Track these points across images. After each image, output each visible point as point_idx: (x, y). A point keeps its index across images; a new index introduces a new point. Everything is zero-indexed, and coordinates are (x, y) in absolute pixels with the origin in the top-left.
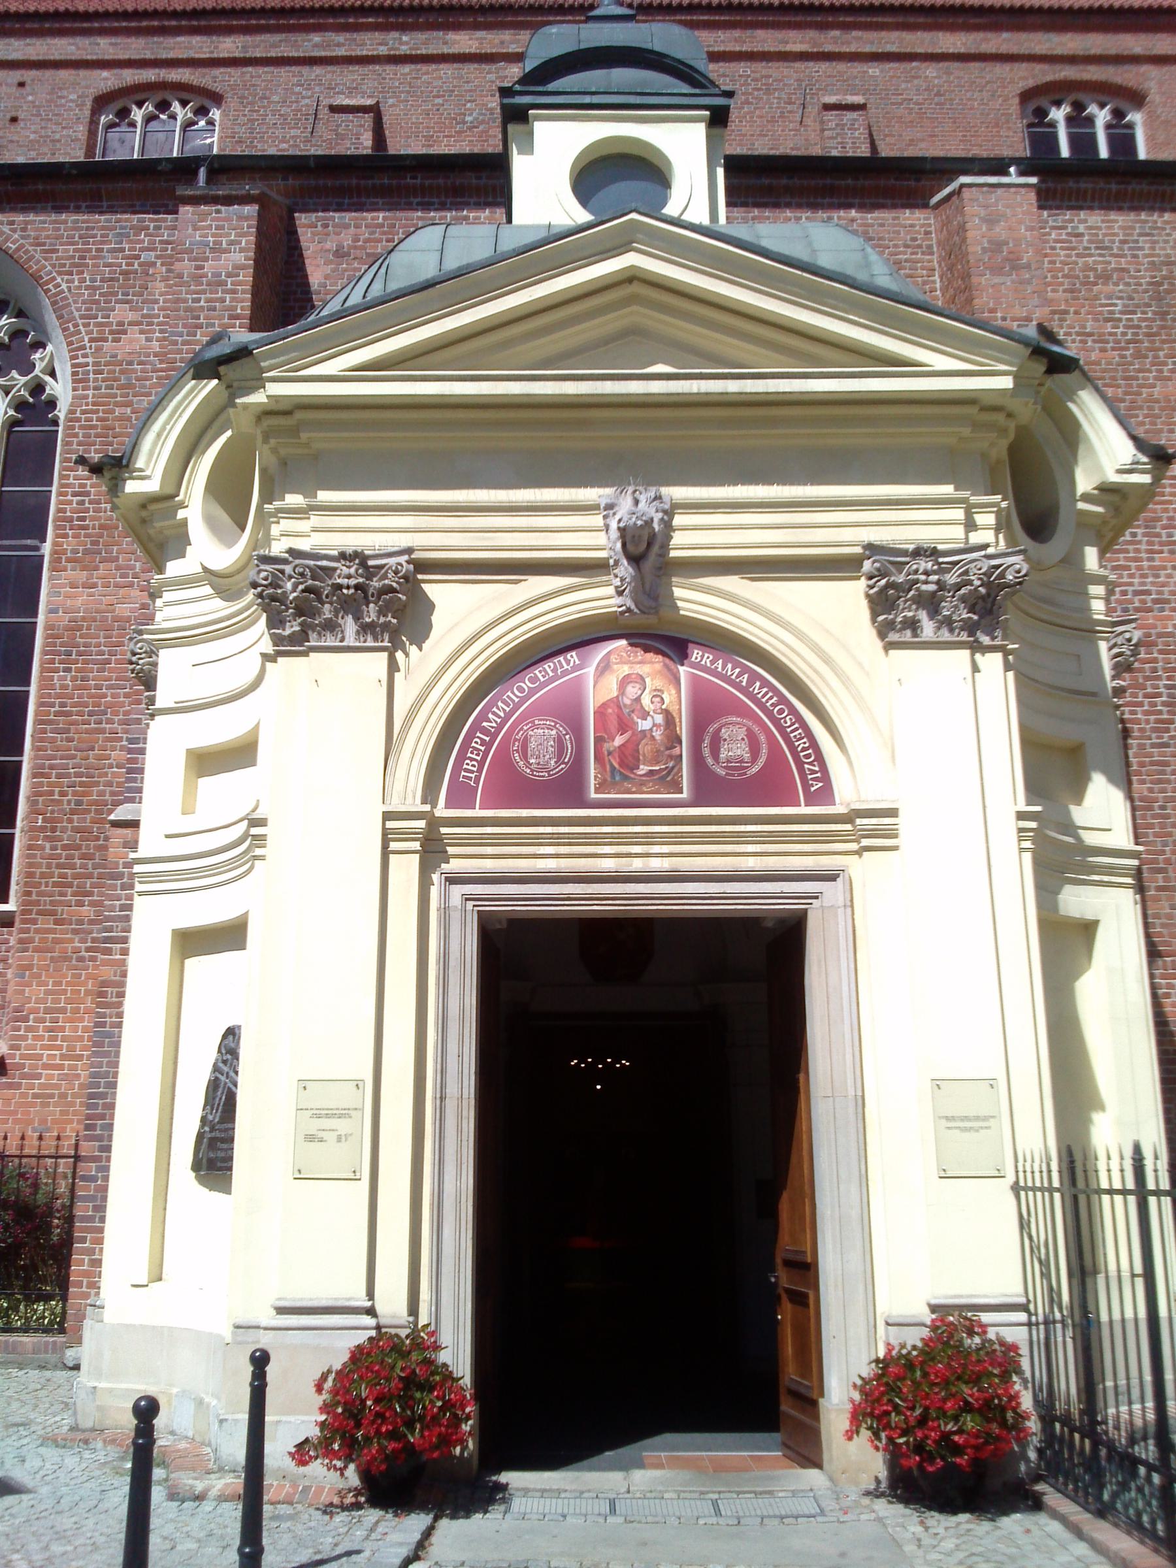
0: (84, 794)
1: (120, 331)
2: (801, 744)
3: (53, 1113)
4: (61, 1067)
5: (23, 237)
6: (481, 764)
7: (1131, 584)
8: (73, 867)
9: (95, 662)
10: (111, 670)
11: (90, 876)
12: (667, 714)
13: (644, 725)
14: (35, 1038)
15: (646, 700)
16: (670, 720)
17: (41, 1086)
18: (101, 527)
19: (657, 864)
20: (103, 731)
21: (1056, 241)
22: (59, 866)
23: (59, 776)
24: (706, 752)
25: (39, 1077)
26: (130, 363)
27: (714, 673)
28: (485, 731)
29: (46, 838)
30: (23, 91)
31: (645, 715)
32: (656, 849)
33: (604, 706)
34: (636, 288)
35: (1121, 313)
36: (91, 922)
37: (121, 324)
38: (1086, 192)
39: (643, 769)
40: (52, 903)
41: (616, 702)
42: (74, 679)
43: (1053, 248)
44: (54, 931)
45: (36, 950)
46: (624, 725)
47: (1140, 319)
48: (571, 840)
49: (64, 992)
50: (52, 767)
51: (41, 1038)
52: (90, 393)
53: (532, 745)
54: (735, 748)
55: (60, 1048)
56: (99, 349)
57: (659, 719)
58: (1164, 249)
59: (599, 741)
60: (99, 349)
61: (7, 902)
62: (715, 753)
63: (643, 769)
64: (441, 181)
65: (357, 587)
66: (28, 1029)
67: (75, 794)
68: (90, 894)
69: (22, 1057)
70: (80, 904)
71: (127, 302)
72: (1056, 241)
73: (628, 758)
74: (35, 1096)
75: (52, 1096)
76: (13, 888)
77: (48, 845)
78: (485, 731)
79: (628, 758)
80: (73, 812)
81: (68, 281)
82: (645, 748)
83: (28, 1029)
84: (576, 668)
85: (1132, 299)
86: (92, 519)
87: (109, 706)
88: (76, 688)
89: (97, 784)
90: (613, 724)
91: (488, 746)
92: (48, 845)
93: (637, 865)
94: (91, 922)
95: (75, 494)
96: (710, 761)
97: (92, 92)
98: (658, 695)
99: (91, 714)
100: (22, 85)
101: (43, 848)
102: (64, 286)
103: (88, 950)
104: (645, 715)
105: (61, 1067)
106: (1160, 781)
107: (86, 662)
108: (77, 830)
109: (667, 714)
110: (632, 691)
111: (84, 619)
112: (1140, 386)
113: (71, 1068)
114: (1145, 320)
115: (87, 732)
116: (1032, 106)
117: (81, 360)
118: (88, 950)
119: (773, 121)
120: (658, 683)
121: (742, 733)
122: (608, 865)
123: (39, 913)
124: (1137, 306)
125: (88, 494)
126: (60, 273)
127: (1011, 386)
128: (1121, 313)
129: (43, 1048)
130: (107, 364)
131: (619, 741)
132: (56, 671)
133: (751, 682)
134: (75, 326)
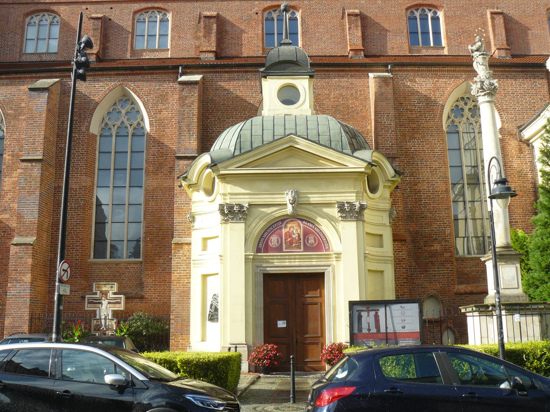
0: (158, 232)
1: (160, 112)
2: (324, 240)
3: (156, 309)
4: (158, 298)
5: (134, 85)
6: (263, 244)
7: (416, 176)
8: (157, 250)
9: (159, 199)
10: (163, 201)
11: (161, 252)
12: (298, 234)
13: (294, 236)
14: (151, 291)
15: (294, 231)
16: (299, 235)
17: (153, 303)
18: (159, 164)
19: (297, 264)
20: (162, 216)
21: (401, 84)
22: (154, 250)
23: (152, 228)
24: (306, 242)
25: (152, 300)
26: (164, 120)
27: (307, 225)
28: (264, 238)
29: (150, 243)
30: (112, 10)
31: (294, 234)
32: (296, 261)
33: (286, 233)
34: (292, 148)
35: (417, 104)
36: (163, 264)
37: (161, 109)
38: (409, 70)
39: (294, 245)
40: (153, 259)
41: (289, 232)
42: (154, 203)
43: (400, 86)
44: (153, 266)
45: (149, 270)
46: (290, 236)
47: (421, 105)
48: (280, 259)
49: (157, 281)
50: (150, 225)
51: (152, 291)
52: (154, 128)
53: (272, 240)
54: (311, 241)
55: (157, 294)
56: (156, 116)
57: (297, 235)
58: (429, 85)
59: (285, 239)
60: (156, 116)
61: (140, 258)
62: (308, 242)
63: (294, 245)
64: (242, 69)
65: (239, 211)
66: (149, 289)
67: (156, 232)
68: (162, 257)
69: (148, 296)
70: (159, 259)
71: (162, 103)
72: (401, 84)
73: (291, 243)
74: (152, 305)
75: (156, 305)
76: (141, 255)
77: (151, 245)
78: (264, 238)
79: (291, 243)
80: (156, 237)
81: (147, 98)
82: (294, 241)
83: (149, 289)
84: (281, 225)
85: (420, 99)
86: (157, 162)
87: (164, 210)
88: (155, 205)
89: (162, 229)
90: (288, 236)
91: (264, 241)
92: (151, 245)
93: (293, 264)
94: (163, 264)
95: (152, 155)
96: (307, 243)
97: (132, 10)
98: (297, 230)
99: (159, 212)
100: (111, 8)
101: (150, 246)
102: (146, 99)
103: (162, 270)
104: (294, 234)
105: (158, 298)
106: (421, 226)
107: (157, 199)
108: (157, 241)
109: (298, 234)
110: (292, 229)
111: (156, 188)
112: (421, 124)
113: (160, 298)
114: (423, 105)
115: (159, 216)
116: (409, 11)
117: (151, 119)
118: (162, 270)
119: (333, 18)
120: (297, 228)
121: (313, 238)
122: (287, 264)
123: (150, 261)
124: (421, 102)
125: (155, 155)
126: (145, 95)
127: (285, 326)
128: (417, 104)
129: (153, 294)
130: (158, 120)
131: (289, 239)
132: (150, 201)
133: (315, 228)
134: (150, 110)
